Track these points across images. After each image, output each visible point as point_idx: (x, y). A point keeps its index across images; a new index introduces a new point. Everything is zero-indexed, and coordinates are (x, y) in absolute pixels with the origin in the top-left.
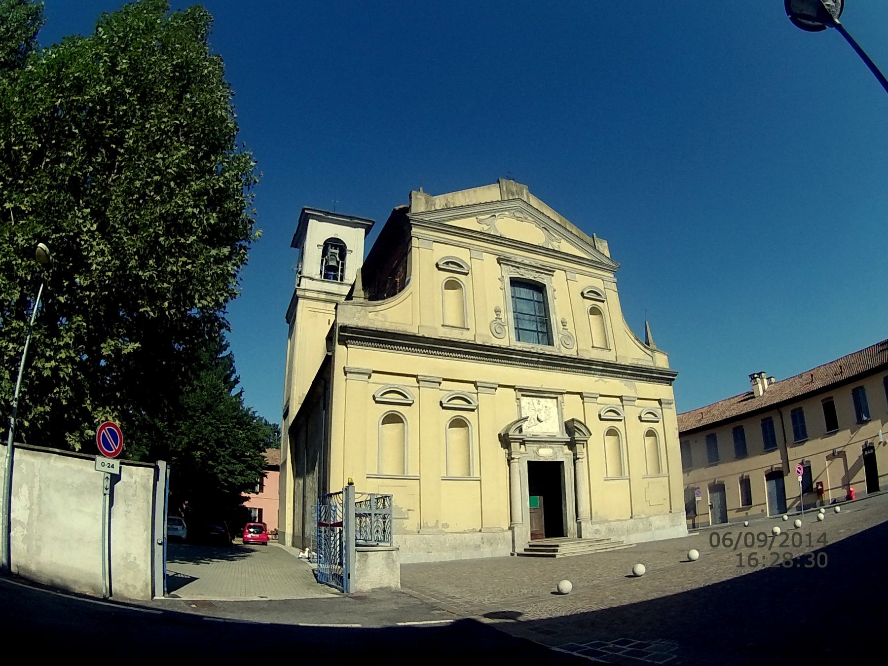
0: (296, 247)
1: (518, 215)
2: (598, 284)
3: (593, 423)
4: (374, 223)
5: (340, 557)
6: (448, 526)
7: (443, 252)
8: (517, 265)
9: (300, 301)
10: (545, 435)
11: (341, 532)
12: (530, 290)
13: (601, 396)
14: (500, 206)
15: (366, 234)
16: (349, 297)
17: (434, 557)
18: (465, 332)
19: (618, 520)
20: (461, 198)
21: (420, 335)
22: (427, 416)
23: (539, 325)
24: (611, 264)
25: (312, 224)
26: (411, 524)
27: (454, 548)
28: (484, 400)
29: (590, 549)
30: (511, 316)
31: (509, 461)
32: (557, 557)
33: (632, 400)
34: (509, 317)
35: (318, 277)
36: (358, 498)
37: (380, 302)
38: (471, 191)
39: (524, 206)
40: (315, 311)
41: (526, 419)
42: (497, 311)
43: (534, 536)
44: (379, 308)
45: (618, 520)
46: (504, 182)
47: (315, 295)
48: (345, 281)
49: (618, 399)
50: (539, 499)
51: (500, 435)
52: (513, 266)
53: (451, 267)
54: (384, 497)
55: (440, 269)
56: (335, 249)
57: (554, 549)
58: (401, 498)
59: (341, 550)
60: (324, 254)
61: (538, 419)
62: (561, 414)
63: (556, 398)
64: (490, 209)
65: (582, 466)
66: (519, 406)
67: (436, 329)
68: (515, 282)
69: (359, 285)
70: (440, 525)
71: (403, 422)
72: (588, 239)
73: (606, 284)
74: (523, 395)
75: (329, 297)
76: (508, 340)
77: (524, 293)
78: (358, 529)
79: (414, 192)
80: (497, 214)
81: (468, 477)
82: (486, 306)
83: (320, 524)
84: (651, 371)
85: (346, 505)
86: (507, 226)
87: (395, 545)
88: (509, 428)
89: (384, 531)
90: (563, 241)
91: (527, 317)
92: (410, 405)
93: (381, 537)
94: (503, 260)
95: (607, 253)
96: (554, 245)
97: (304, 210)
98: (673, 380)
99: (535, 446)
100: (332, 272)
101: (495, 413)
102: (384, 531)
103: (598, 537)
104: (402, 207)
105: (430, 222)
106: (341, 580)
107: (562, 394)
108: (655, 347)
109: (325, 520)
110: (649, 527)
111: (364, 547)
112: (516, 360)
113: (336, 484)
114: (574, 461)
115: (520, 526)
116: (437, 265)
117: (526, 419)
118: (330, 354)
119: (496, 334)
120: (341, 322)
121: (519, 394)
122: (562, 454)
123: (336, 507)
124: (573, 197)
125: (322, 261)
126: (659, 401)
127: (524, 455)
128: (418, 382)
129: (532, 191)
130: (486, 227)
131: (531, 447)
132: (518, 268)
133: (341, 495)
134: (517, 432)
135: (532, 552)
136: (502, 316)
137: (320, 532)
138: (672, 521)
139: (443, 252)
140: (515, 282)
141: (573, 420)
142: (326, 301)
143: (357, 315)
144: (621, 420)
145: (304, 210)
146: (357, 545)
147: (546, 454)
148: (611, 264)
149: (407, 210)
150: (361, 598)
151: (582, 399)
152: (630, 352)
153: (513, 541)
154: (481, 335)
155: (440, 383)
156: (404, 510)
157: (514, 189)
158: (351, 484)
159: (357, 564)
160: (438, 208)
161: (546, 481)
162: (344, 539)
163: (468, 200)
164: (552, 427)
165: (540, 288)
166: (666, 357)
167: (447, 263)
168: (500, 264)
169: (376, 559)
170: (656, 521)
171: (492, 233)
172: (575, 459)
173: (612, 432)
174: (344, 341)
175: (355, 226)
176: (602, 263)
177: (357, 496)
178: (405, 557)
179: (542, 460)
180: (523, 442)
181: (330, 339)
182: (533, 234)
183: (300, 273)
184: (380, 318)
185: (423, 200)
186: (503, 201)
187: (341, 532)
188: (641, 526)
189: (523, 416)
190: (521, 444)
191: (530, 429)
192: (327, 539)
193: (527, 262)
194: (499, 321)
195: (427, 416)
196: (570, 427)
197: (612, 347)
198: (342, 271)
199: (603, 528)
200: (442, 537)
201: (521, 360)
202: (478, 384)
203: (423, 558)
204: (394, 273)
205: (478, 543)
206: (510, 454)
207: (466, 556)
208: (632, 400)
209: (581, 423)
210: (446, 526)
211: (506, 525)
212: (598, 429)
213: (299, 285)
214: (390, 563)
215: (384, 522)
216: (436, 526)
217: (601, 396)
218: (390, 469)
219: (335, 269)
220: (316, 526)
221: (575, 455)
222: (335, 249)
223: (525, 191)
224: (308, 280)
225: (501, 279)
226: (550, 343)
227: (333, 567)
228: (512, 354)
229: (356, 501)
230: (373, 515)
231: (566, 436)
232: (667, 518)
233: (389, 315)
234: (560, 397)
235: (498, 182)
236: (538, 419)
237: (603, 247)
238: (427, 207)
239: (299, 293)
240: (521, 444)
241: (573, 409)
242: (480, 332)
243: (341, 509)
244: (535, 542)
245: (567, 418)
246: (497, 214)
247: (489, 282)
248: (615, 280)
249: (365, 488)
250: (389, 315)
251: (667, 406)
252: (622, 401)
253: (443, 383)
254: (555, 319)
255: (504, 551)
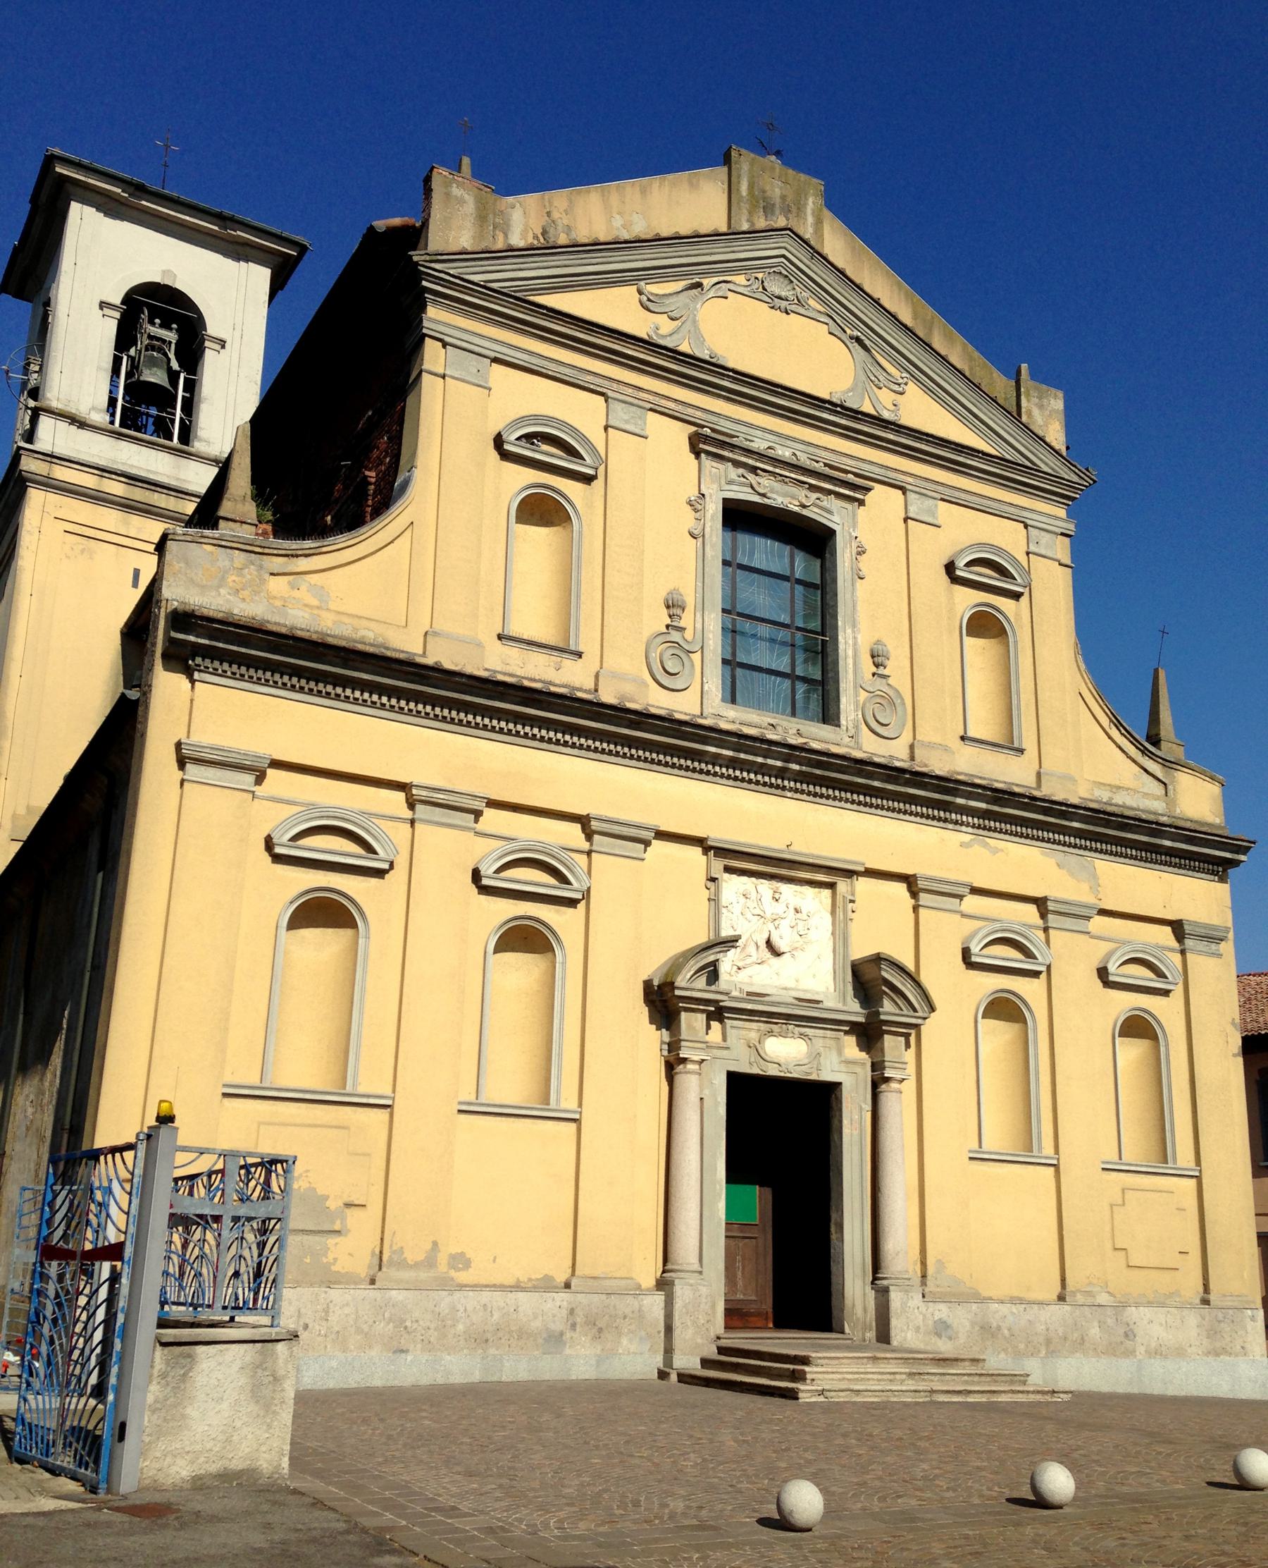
0: (20, 295)
1: (776, 287)
2: (1007, 538)
3: (942, 976)
4: (303, 249)
5: (103, 1366)
6: (467, 1264)
7: (520, 398)
8: (755, 461)
9: (35, 497)
10: (788, 997)
11: (115, 1278)
12: (781, 542)
13: (1103, 912)
14: (719, 252)
15: (277, 286)
16: (208, 512)
17: (414, 1370)
18: (568, 663)
19: (1015, 1301)
20: (597, 211)
21: (429, 661)
22: (431, 909)
23: (800, 656)
24: (1065, 473)
25: (85, 227)
26: (351, 1251)
27: (480, 1340)
28: (609, 875)
29: (911, 1385)
30: (714, 623)
31: (672, 1065)
32: (804, 1398)
33: (1078, 914)
34: (708, 627)
35: (101, 418)
36: (185, 1164)
37: (308, 544)
38: (631, 187)
39: (800, 256)
40: (87, 534)
41: (731, 942)
42: (673, 605)
43: (736, 1316)
44: (303, 564)
45: (1015, 1301)
46: (745, 161)
47: (87, 480)
48: (198, 446)
49: (1032, 909)
50: (755, 1197)
51: (648, 985)
52: (737, 464)
53: (546, 453)
54: (269, 1164)
55: (505, 456)
56: (159, 321)
57: (795, 1367)
58: (325, 1160)
59: (106, 1343)
60: (125, 338)
61: (768, 942)
62: (841, 936)
63: (832, 886)
64: (683, 260)
65: (899, 1104)
66: (714, 901)
67: (479, 645)
68: (739, 517)
69: (241, 480)
70: (442, 1259)
71: (353, 925)
72: (1000, 385)
73: (1035, 539)
74: (728, 869)
75: (139, 494)
76: (698, 697)
77: (765, 552)
78: (173, 1269)
79: (440, 176)
80: (707, 282)
81: (539, 1110)
82: (641, 578)
83: (48, 1252)
84: (1153, 827)
85: (143, 1190)
86: (741, 328)
87: (287, 1321)
88: (677, 964)
89: (258, 1274)
90: (912, 388)
91: (764, 630)
92: (379, 873)
93: (245, 1293)
94: (706, 439)
95: (1056, 435)
96: (882, 402)
97: (50, 160)
98: (1235, 863)
99: (752, 1030)
100: (153, 406)
101: (640, 914)
102: (258, 1274)
103: (945, 1347)
104: (396, 221)
105: (486, 290)
106: (91, 1449)
107: (850, 874)
108: (1178, 753)
109: (64, 1236)
110: (1122, 1342)
111: (183, 1331)
112: (715, 760)
113: (116, 1119)
114: (875, 1085)
115: (693, 1279)
116: (499, 442)
117: (731, 942)
118: (133, 694)
119: (664, 677)
120: (175, 594)
121: (718, 865)
122: (839, 1062)
123: (109, 1191)
124: (972, 242)
125: (117, 362)
126: (1178, 928)
127: (718, 1052)
128: (411, 806)
129: (837, 204)
130: (666, 326)
131: (741, 1033)
132: (754, 470)
133: (129, 1155)
134: (701, 982)
135: (728, 1373)
136: (687, 620)
137: (44, 1277)
138: (1213, 1333)
139: (520, 398)
140: (739, 517)
141: (878, 959)
142: (128, 506)
143: (231, 578)
144: (1036, 974)
145: (50, 160)
146: (163, 1324)
147: (786, 1054)
148: (1065, 473)
149: (414, 235)
150: (153, 1511)
151: (914, 894)
152: (1089, 760)
153: (669, 1329)
154: (615, 675)
155: (478, 814)
156: (333, 1204)
157: (776, 190)
158: (166, 1119)
159: (154, 1388)
160: (517, 240)
161: (784, 1146)
162: (122, 1303)
163: (618, 222)
164: (813, 974)
165: (815, 540)
166: (1215, 789)
167: (529, 437)
168: (697, 453)
169: (220, 1370)
170: (1152, 1325)
171: (684, 348)
172: (878, 1082)
173: (1004, 1008)
174: (180, 659)
175: (238, 252)
176: (1033, 470)
177: (181, 1158)
178: (321, 1366)
179: (773, 1071)
180: (718, 1013)
181: (136, 633)
182: (810, 356)
183: (35, 393)
184: (304, 594)
185: (470, 206)
186: (732, 234)
187: (115, 1278)
188: (1095, 1332)
189: (726, 932)
190: (711, 1017)
191: (741, 974)
192: (65, 1301)
193: (784, 453)
194: (675, 636)
195: (431, 909)
196: (868, 979)
197: (1029, 743)
198: (189, 407)
199: (961, 1318)
200: (445, 1301)
201: (733, 763)
202: (595, 825)
203: (376, 1370)
204: (361, 453)
205: (558, 1326)
206: (674, 1046)
207: (517, 1367)
208: (1078, 914)
209: (901, 969)
210: (460, 1261)
211: (648, 1272)
212: (956, 994)
213: (30, 436)
214: (261, 1387)
215: (262, 1246)
216: (430, 1261)
217: (1103, 912)
218: (302, 1067)
219: (163, 398)
220: (32, 1256)
221: (877, 1066)
222: (159, 321)
223: (812, 203)
224: (63, 426)
225: (696, 504)
226: (829, 715)
227: (74, 1403)
228: (704, 740)
229: (178, 1173)
230: (227, 1222)
231: (855, 1006)
232: (1192, 1319)
233: (342, 588)
234: (843, 885)
235: (727, 160)
236: (768, 942)
237: (1048, 415)
238: (480, 236)
239: (29, 465)
240: (711, 1017)
241: (882, 922)
242: (616, 668)
243: (123, 1199)
244: (741, 1340)
245: (861, 950)
246: (707, 282)
247: (657, 505)
248: (1070, 527)
249: (215, 1130)
250: (342, 588)
251: (1202, 945)
252: (1043, 915)
253: (489, 813)
254: (852, 644)
255: (636, 1359)
